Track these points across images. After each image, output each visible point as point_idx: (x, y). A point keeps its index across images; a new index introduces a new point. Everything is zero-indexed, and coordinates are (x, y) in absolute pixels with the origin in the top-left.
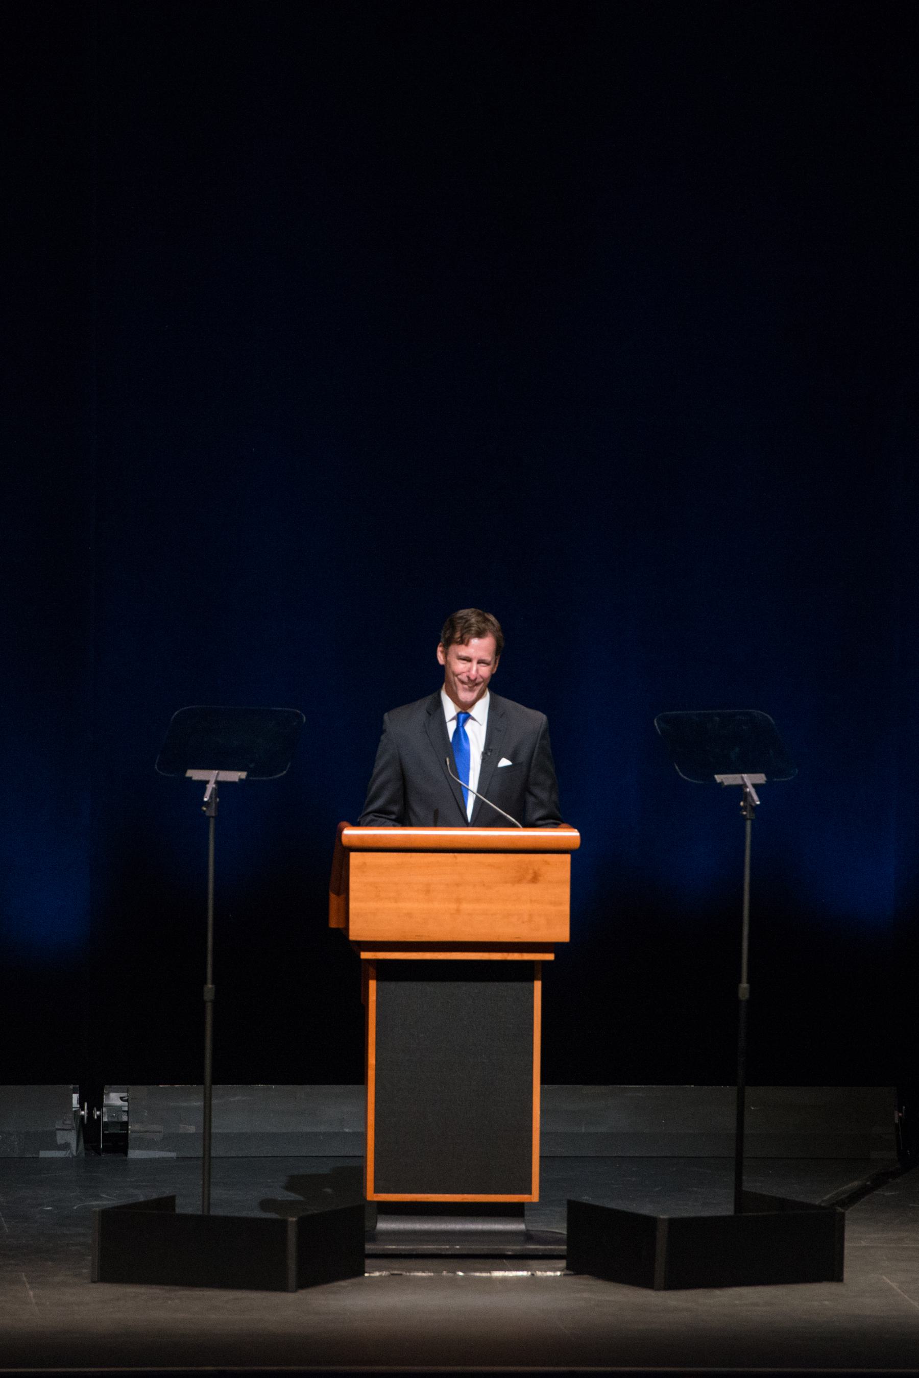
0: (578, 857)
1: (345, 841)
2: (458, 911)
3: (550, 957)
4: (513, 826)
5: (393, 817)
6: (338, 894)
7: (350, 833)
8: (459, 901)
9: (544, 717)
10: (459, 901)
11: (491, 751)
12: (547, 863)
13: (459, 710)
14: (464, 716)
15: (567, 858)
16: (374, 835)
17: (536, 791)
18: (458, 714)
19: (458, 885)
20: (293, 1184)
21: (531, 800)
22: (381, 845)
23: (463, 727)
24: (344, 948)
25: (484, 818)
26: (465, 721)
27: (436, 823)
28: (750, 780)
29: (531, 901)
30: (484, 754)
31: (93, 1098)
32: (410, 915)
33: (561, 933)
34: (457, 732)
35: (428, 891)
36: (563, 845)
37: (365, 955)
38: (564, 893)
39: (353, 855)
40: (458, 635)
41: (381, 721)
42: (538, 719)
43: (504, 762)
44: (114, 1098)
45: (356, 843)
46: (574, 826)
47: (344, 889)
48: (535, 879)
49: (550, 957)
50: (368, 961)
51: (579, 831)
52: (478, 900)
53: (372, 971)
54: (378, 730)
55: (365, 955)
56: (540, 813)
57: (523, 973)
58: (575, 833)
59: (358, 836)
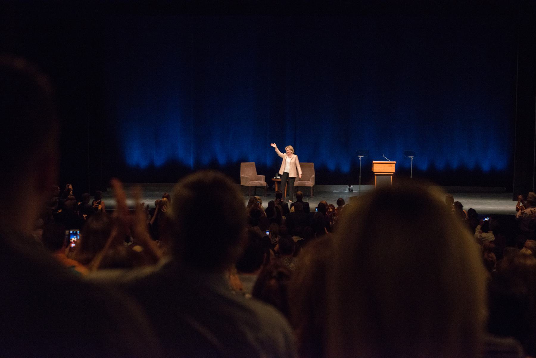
7: (374, 162)
20: (332, 193)
28: (412, 157)
31: (350, 186)
33: (394, 171)
44: (352, 186)
57: (390, 175)
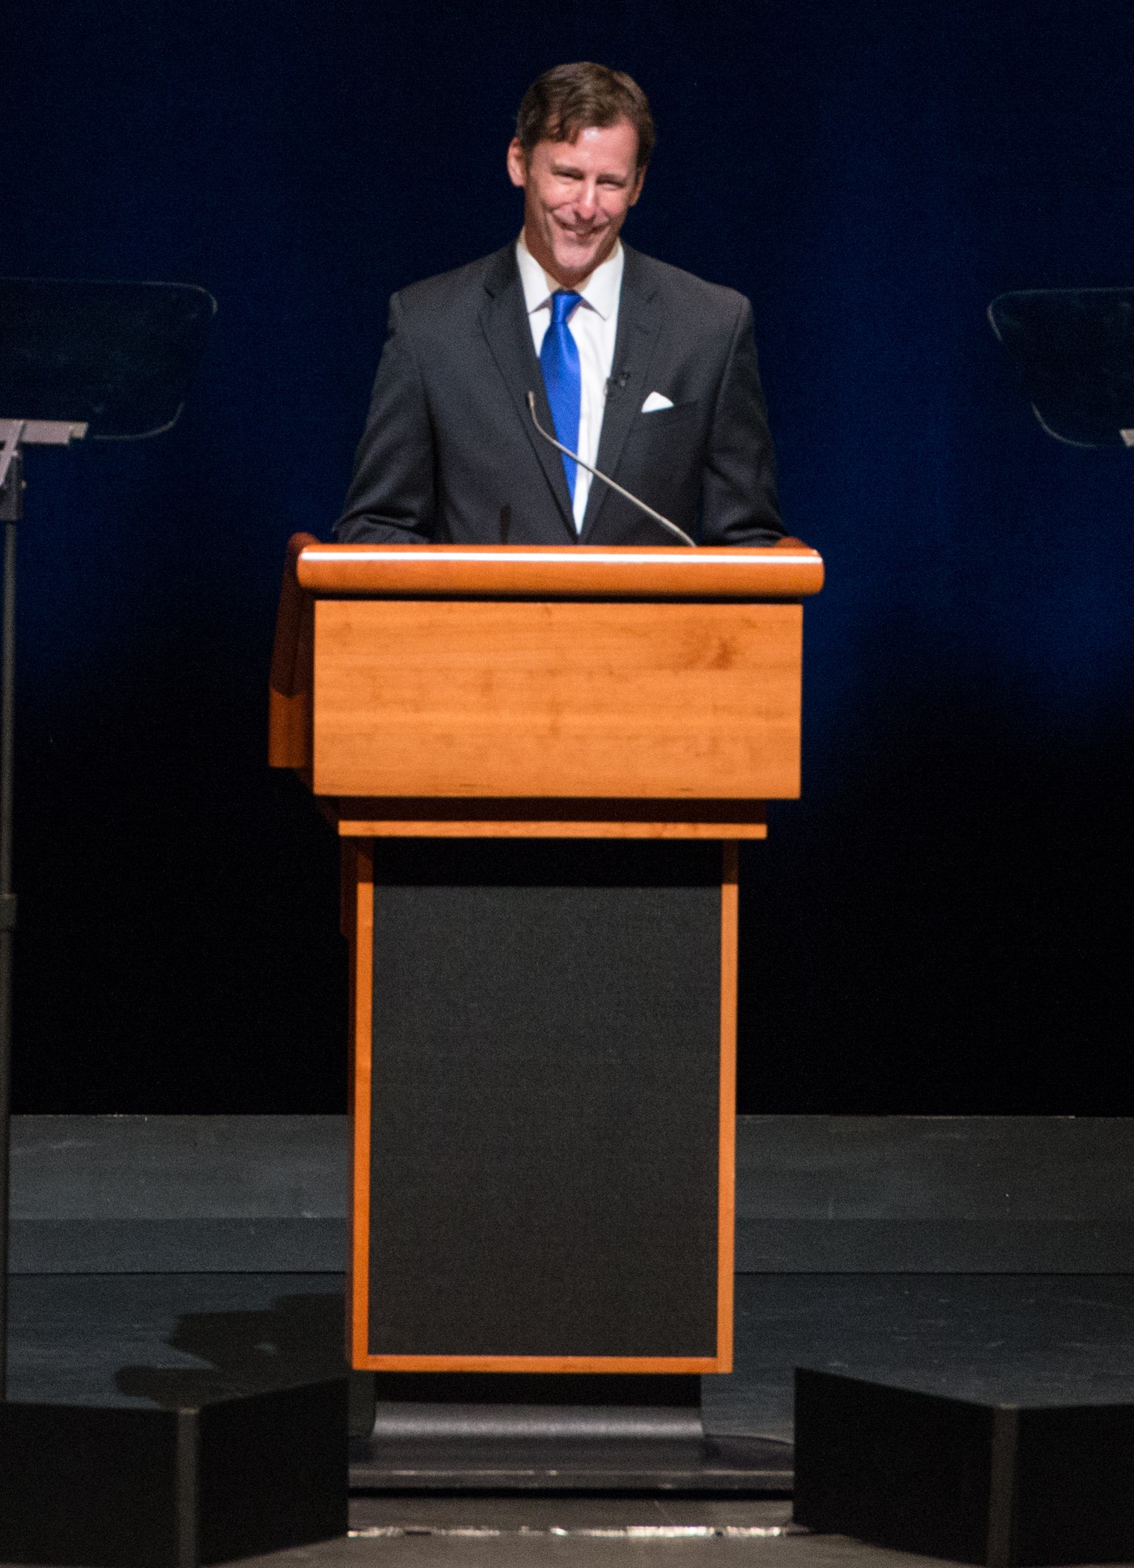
0: (819, 611)
2: (554, 730)
3: (758, 832)
5: (411, 522)
8: (555, 707)
9: (745, 302)
10: (555, 707)
12: (750, 624)
14: (567, 299)
15: (796, 612)
16: (370, 564)
17: (727, 464)
18: (555, 296)
19: (553, 672)
21: (715, 484)
22: (383, 584)
23: (565, 323)
24: (299, 817)
25: (612, 525)
26: (570, 309)
27: (506, 533)
29: (715, 708)
30: (613, 384)
32: (447, 739)
34: (551, 334)
36: (786, 585)
37: (349, 828)
38: (787, 692)
39: (321, 606)
41: (386, 311)
42: (731, 305)
43: (656, 402)
45: (329, 581)
46: (809, 541)
48: (724, 659)
49: (758, 832)
52: (598, 707)
53: (364, 864)
55: (349, 828)
56: (735, 514)
58: (812, 559)
59: (333, 565)
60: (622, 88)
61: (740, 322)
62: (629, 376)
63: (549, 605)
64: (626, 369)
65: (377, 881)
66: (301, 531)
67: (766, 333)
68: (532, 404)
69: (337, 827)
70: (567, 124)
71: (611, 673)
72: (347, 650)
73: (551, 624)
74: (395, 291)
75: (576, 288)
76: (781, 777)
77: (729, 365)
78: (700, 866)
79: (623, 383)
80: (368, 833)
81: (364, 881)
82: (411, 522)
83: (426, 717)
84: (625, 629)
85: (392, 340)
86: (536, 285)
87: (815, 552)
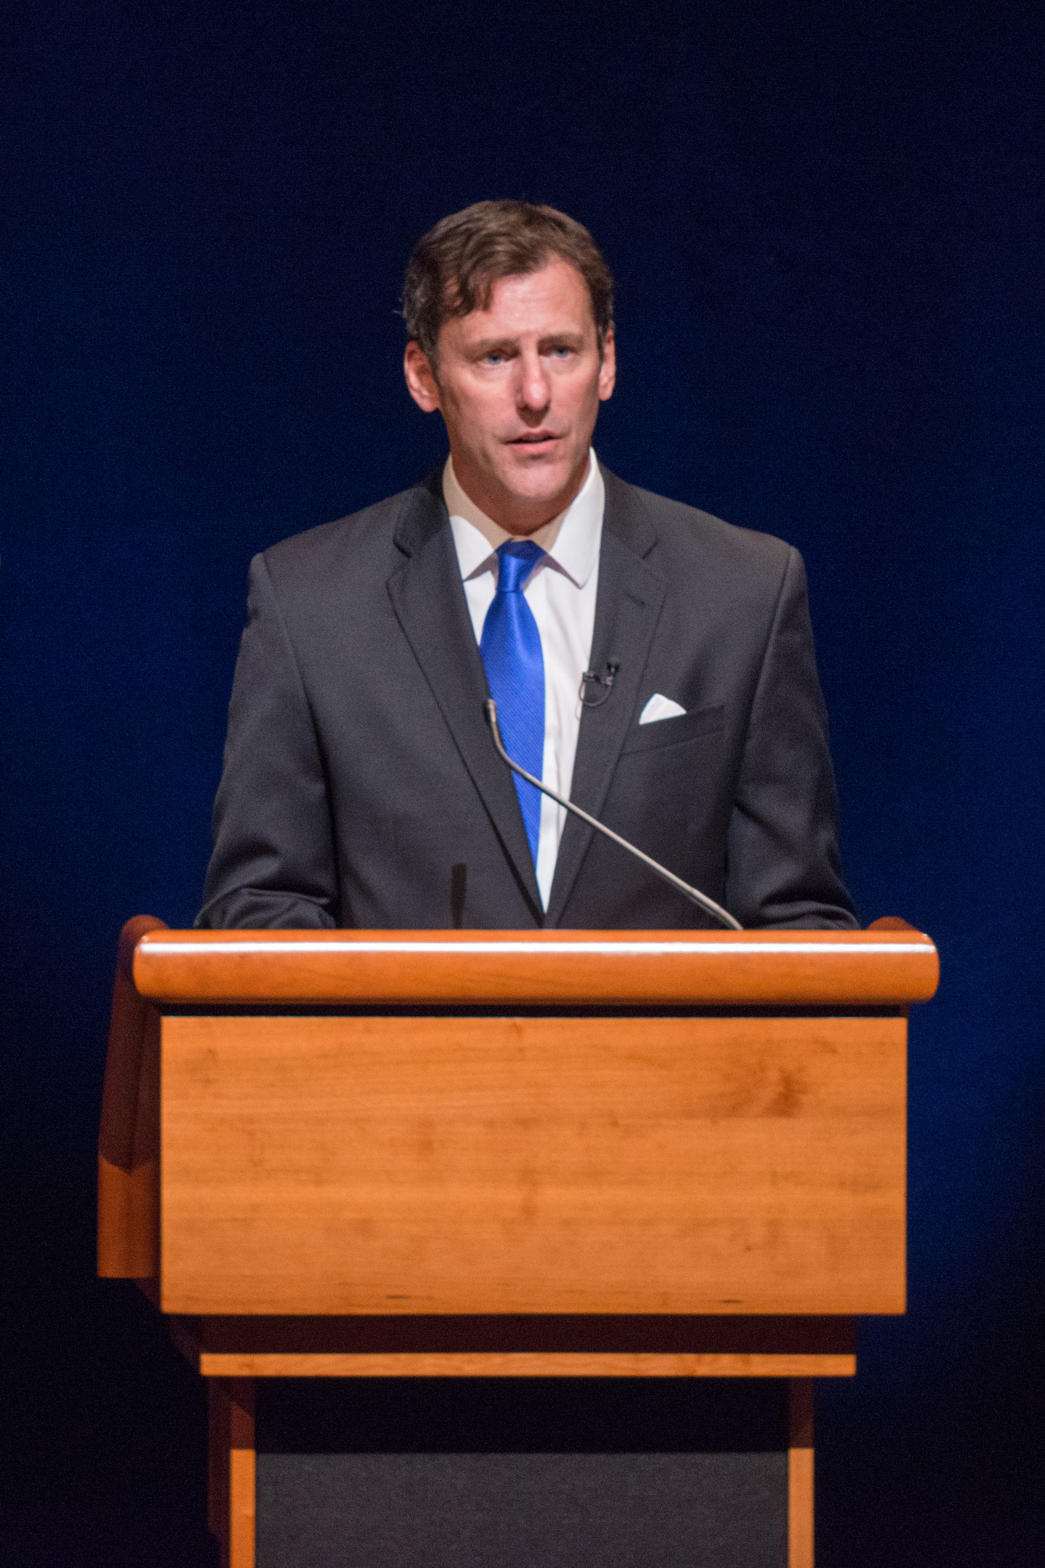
0: (932, 1026)
1: (144, 978)
2: (529, 1211)
3: (841, 1365)
4: (713, 924)
5: (324, 901)
6: (128, 1164)
8: (529, 1176)
9: (794, 553)
10: (529, 1176)
11: (615, 669)
12: (826, 1047)
13: (503, 536)
14: (521, 556)
15: (897, 1028)
16: (244, 957)
17: (767, 801)
18: (503, 551)
19: (524, 1123)
21: (745, 832)
22: (264, 990)
23: (518, 591)
24: (148, 1343)
25: (599, 896)
26: (524, 574)
27: (458, 913)
29: (774, 1175)
30: (592, 682)
32: (365, 1226)
34: (497, 610)
35: (426, 1146)
36: (883, 988)
37: (215, 1364)
38: (888, 1147)
39: (170, 1025)
40: (452, 288)
41: (243, 584)
42: (771, 562)
43: (661, 708)
45: (183, 986)
46: (918, 921)
47: (144, 1150)
48: (788, 1101)
49: (841, 1365)
50: (225, 1383)
51: (936, 940)
52: (594, 1175)
53: (241, 1420)
54: (224, 615)
55: (215, 1364)
56: (782, 874)
58: (924, 947)
59: (189, 960)
60: (546, 219)
61: (788, 583)
62: (617, 668)
63: (518, 1020)
64: (614, 660)
65: (261, 1447)
66: (138, 912)
67: (828, 599)
68: (493, 719)
69: (197, 1362)
70: (472, 283)
71: (615, 1124)
72: (209, 1088)
73: (521, 1050)
74: (259, 551)
75: (536, 538)
76: (877, 1281)
77: (770, 650)
78: (754, 1418)
79: (609, 680)
80: (246, 1372)
81: (242, 1446)
82: (324, 901)
83: (333, 1193)
84: (633, 1056)
85: (254, 624)
86: (473, 541)
87: (925, 936)
